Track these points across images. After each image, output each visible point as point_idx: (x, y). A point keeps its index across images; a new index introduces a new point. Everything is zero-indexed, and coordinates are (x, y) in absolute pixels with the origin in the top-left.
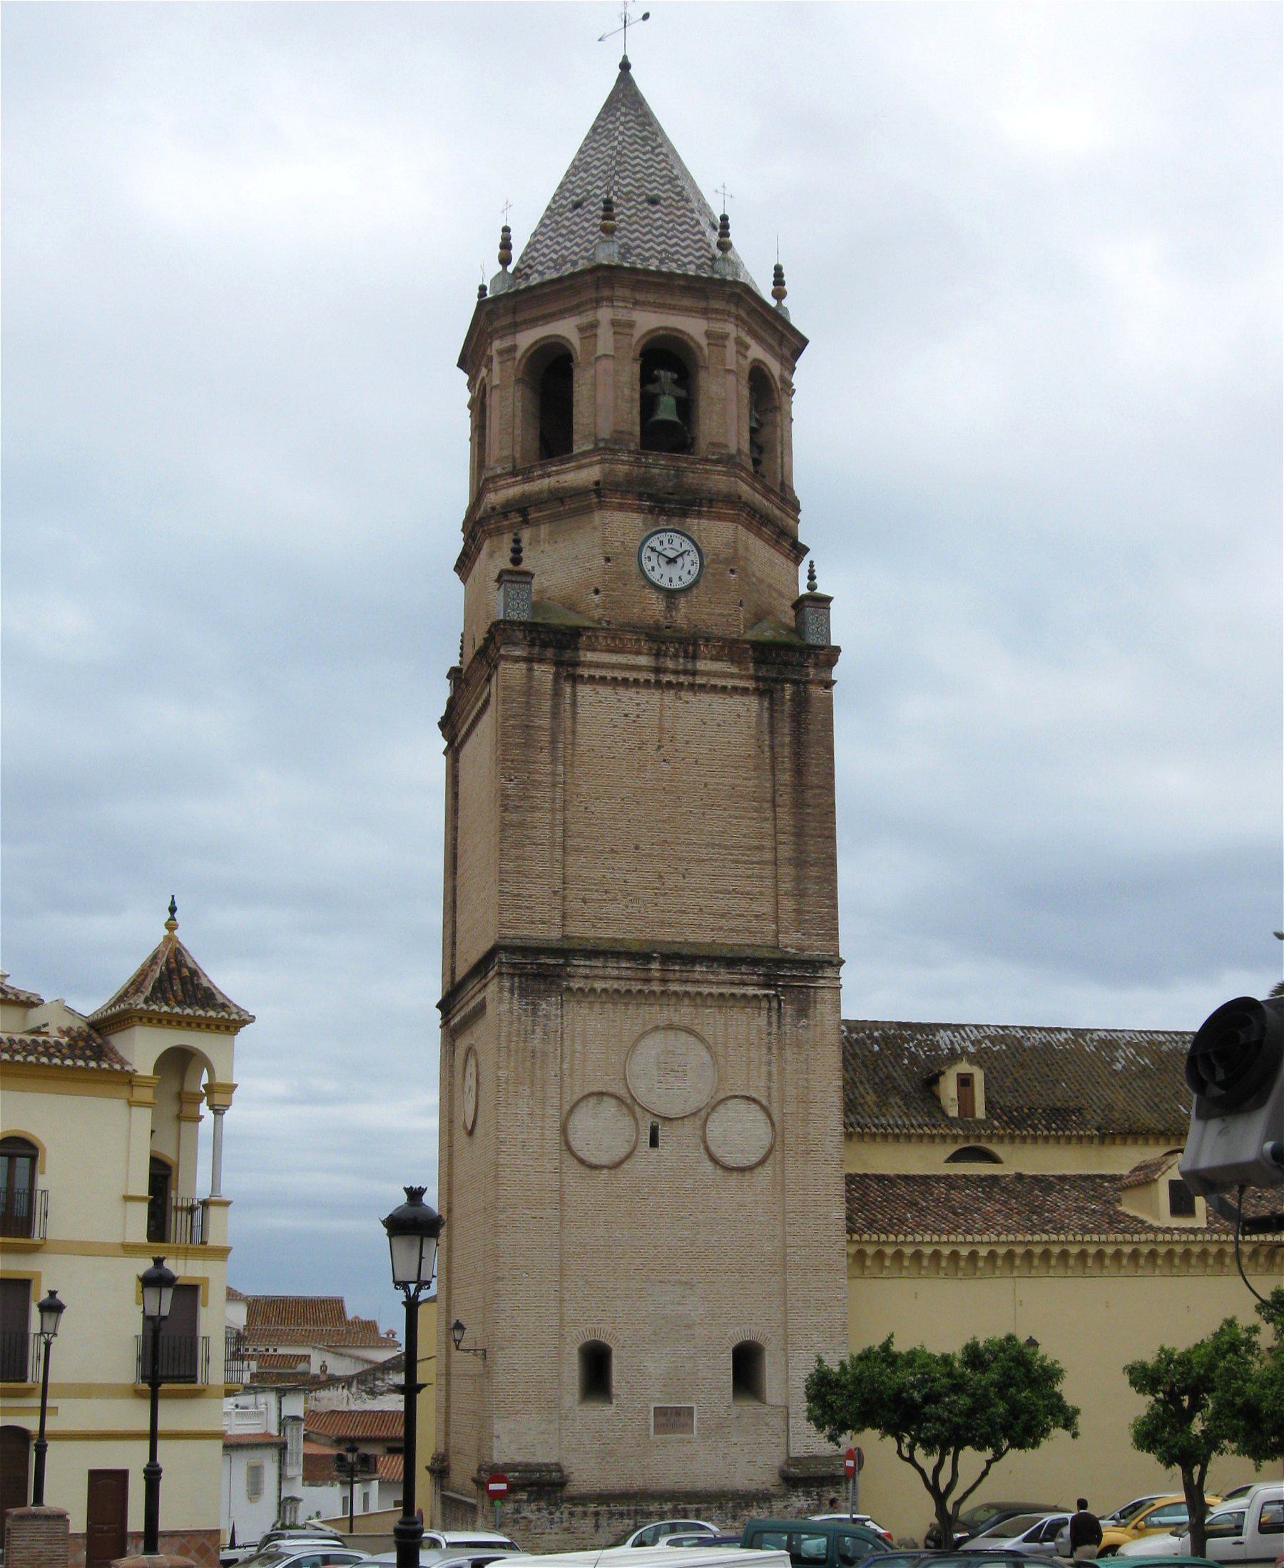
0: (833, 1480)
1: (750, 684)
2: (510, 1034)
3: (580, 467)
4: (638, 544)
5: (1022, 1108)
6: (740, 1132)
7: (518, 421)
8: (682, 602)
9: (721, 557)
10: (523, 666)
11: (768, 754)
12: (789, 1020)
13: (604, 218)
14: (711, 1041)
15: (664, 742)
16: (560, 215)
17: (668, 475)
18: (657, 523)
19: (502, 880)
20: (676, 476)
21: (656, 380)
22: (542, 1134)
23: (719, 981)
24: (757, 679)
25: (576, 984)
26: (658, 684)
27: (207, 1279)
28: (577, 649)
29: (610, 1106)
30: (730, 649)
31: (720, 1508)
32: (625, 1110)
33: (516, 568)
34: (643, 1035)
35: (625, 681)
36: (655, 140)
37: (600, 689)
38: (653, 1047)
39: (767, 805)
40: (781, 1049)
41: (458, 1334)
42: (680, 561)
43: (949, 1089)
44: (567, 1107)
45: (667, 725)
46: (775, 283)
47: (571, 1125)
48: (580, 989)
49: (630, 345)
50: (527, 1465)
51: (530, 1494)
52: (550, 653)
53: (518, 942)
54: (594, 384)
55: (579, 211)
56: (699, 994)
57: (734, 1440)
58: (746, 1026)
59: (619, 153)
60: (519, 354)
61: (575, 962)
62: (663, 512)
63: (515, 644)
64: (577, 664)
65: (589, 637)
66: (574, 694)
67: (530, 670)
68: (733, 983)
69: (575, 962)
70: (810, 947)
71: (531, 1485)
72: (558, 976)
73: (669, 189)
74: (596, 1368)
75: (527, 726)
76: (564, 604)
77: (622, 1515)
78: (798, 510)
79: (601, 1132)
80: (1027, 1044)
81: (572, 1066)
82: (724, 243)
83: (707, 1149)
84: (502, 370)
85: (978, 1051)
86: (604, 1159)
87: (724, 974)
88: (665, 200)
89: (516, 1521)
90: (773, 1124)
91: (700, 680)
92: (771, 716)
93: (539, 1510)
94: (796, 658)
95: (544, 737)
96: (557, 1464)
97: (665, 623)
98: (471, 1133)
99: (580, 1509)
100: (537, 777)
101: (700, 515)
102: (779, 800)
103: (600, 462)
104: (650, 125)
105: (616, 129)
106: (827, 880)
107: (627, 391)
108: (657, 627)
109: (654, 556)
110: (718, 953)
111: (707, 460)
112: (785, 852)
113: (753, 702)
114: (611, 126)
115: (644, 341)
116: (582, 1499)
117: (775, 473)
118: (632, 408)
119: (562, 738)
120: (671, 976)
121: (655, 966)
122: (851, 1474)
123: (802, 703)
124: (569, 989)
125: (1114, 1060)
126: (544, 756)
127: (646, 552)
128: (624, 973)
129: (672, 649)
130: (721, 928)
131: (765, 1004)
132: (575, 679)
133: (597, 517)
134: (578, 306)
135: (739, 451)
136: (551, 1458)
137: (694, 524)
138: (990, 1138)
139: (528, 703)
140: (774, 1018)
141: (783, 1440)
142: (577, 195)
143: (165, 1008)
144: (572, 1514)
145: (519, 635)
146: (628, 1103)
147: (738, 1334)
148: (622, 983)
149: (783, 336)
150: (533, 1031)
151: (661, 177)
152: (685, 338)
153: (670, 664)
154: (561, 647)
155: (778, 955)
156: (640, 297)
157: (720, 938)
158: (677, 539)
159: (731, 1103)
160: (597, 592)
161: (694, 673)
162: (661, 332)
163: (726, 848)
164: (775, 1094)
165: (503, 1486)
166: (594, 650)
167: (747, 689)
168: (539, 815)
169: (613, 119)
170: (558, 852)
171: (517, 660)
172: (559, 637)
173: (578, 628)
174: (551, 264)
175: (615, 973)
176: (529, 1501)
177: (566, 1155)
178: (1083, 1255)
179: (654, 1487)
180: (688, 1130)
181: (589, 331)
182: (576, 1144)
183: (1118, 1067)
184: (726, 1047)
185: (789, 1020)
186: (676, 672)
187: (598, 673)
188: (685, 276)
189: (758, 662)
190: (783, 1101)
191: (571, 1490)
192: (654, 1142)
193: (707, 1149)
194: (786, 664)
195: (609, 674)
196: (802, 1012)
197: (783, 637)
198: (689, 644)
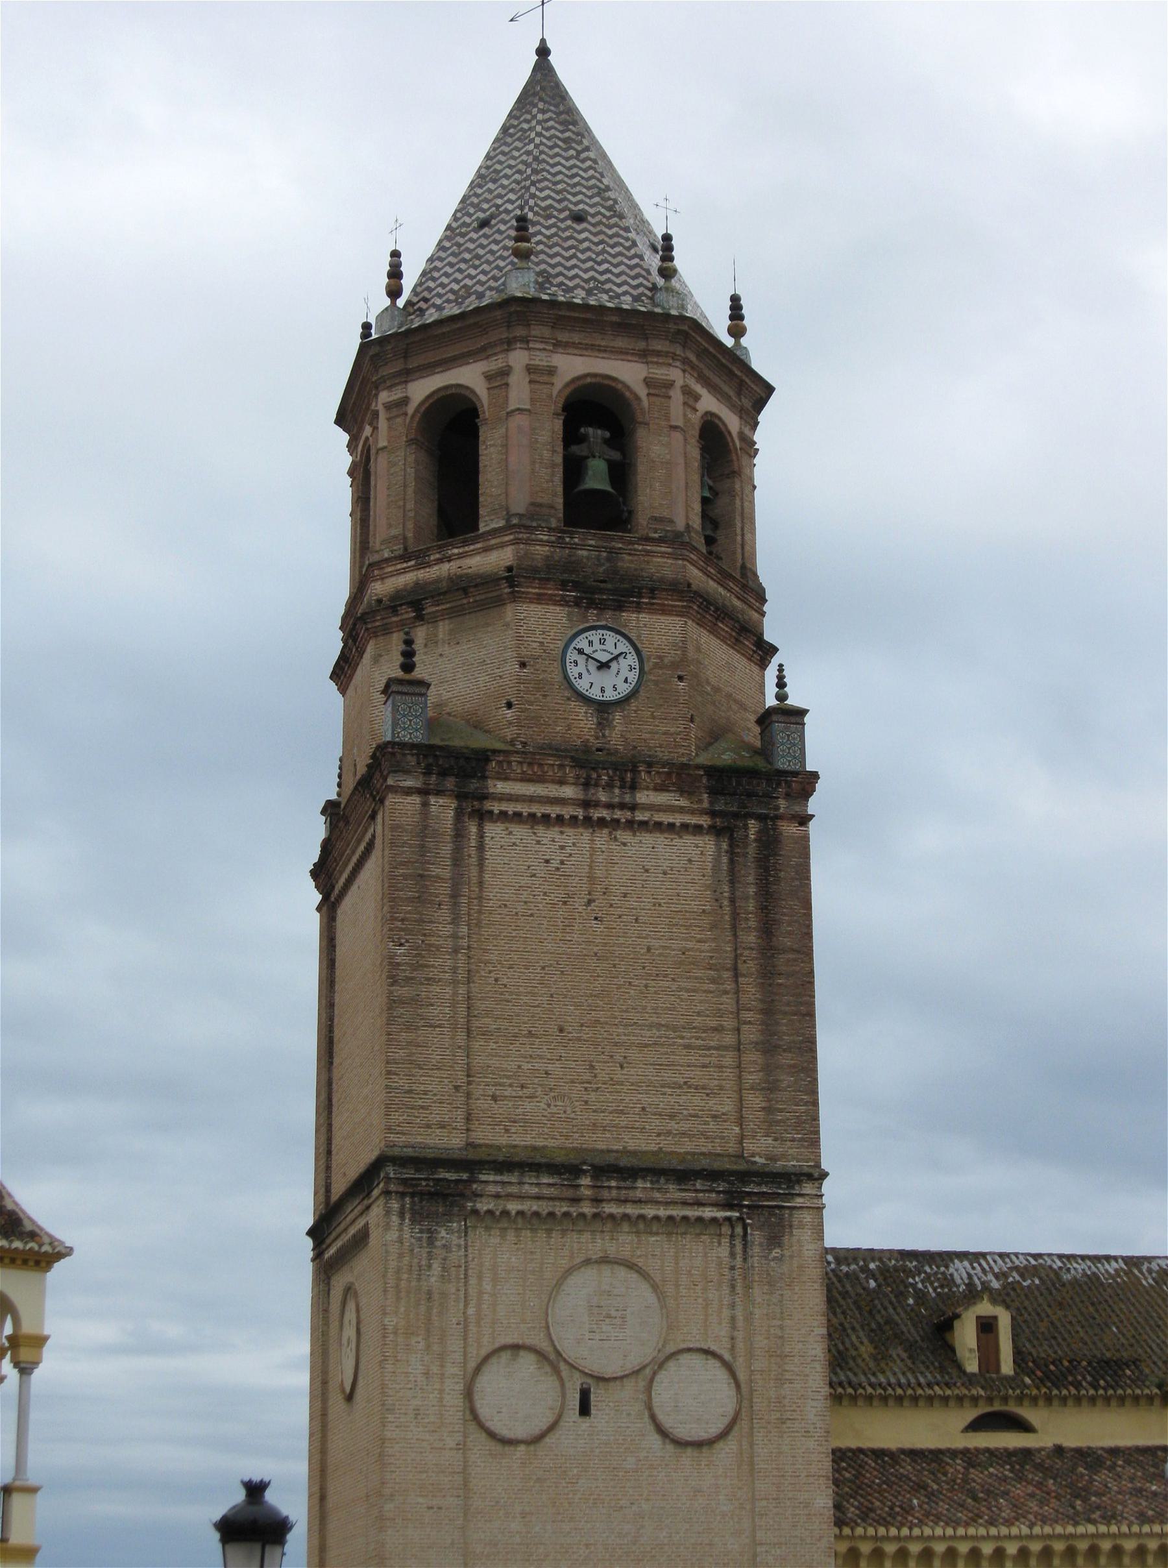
2: (398, 1270)
3: (486, 550)
4: (561, 644)
6: (696, 1396)
7: (410, 491)
9: (666, 661)
10: (417, 799)
14: (658, 1278)
15: (596, 895)
17: (598, 558)
18: (585, 619)
19: (389, 1073)
20: (608, 560)
21: (582, 439)
22: (441, 1399)
23: (666, 1203)
24: (713, 814)
25: (483, 1206)
26: (588, 821)
28: (484, 778)
29: (527, 1362)
30: (679, 776)
32: (548, 1369)
33: (407, 677)
34: (569, 1272)
35: (546, 818)
36: (581, 142)
39: (726, 975)
40: (748, 1287)
42: (614, 665)
43: (966, 1336)
44: (472, 1365)
45: (598, 873)
46: (732, 318)
48: (490, 1212)
52: (450, 783)
53: (409, 1152)
55: (486, 230)
56: (642, 1217)
58: (705, 1256)
59: (536, 159)
60: (411, 409)
61: (483, 1177)
62: (592, 604)
63: (407, 772)
64: (485, 797)
65: (500, 763)
66: (481, 836)
67: (425, 804)
68: (685, 1203)
69: (483, 1177)
70: (784, 1156)
72: (462, 1195)
75: (421, 876)
76: (468, 721)
78: (763, 600)
79: (517, 1396)
83: (653, 1417)
85: (1004, 1287)
86: (520, 1431)
87: (673, 1191)
91: (640, 816)
92: (731, 861)
95: (442, 890)
100: (433, 940)
101: (639, 608)
102: (742, 968)
103: (516, 542)
104: (575, 123)
105: (530, 129)
106: (804, 1070)
109: (581, 660)
110: (665, 1164)
111: (647, 539)
112: (751, 1034)
113: (708, 844)
114: (525, 126)
117: (734, 553)
118: (553, 475)
119: (465, 890)
120: (605, 1194)
121: (585, 1181)
123: (770, 844)
124: (475, 1212)
126: (445, 913)
127: (572, 655)
128: (546, 1191)
129: (605, 776)
130: (669, 1133)
131: (726, 1230)
132: (483, 816)
134: (484, 349)
137: (631, 619)
138: (1020, 1400)
139: (423, 846)
142: (484, 211)
145: (412, 760)
146: (552, 1360)
149: (741, 383)
150: (430, 1266)
152: (619, 386)
153: (603, 797)
154: (464, 775)
155: (742, 1166)
156: (563, 336)
159: (685, 1358)
160: (509, 705)
161: (633, 807)
163: (675, 1029)
164: (740, 1345)
166: (506, 779)
169: (528, 117)
170: (461, 1037)
171: (408, 792)
172: (462, 762)
174: (452, 297)
175: (535, 1190)
177: (472, 1426)
180: (629, 1392)
181: (499, 379)
182: (484, 1412)
184: (677, 1286)
186: (610, 806)
187: (510, 808)
188: (619, 310)
189: (714, 792)
193: (653, 1417)
194: (750, 795)
195: (524, 809)
196: (774, 1240)
197: (746, 760)
198: (627, 770)
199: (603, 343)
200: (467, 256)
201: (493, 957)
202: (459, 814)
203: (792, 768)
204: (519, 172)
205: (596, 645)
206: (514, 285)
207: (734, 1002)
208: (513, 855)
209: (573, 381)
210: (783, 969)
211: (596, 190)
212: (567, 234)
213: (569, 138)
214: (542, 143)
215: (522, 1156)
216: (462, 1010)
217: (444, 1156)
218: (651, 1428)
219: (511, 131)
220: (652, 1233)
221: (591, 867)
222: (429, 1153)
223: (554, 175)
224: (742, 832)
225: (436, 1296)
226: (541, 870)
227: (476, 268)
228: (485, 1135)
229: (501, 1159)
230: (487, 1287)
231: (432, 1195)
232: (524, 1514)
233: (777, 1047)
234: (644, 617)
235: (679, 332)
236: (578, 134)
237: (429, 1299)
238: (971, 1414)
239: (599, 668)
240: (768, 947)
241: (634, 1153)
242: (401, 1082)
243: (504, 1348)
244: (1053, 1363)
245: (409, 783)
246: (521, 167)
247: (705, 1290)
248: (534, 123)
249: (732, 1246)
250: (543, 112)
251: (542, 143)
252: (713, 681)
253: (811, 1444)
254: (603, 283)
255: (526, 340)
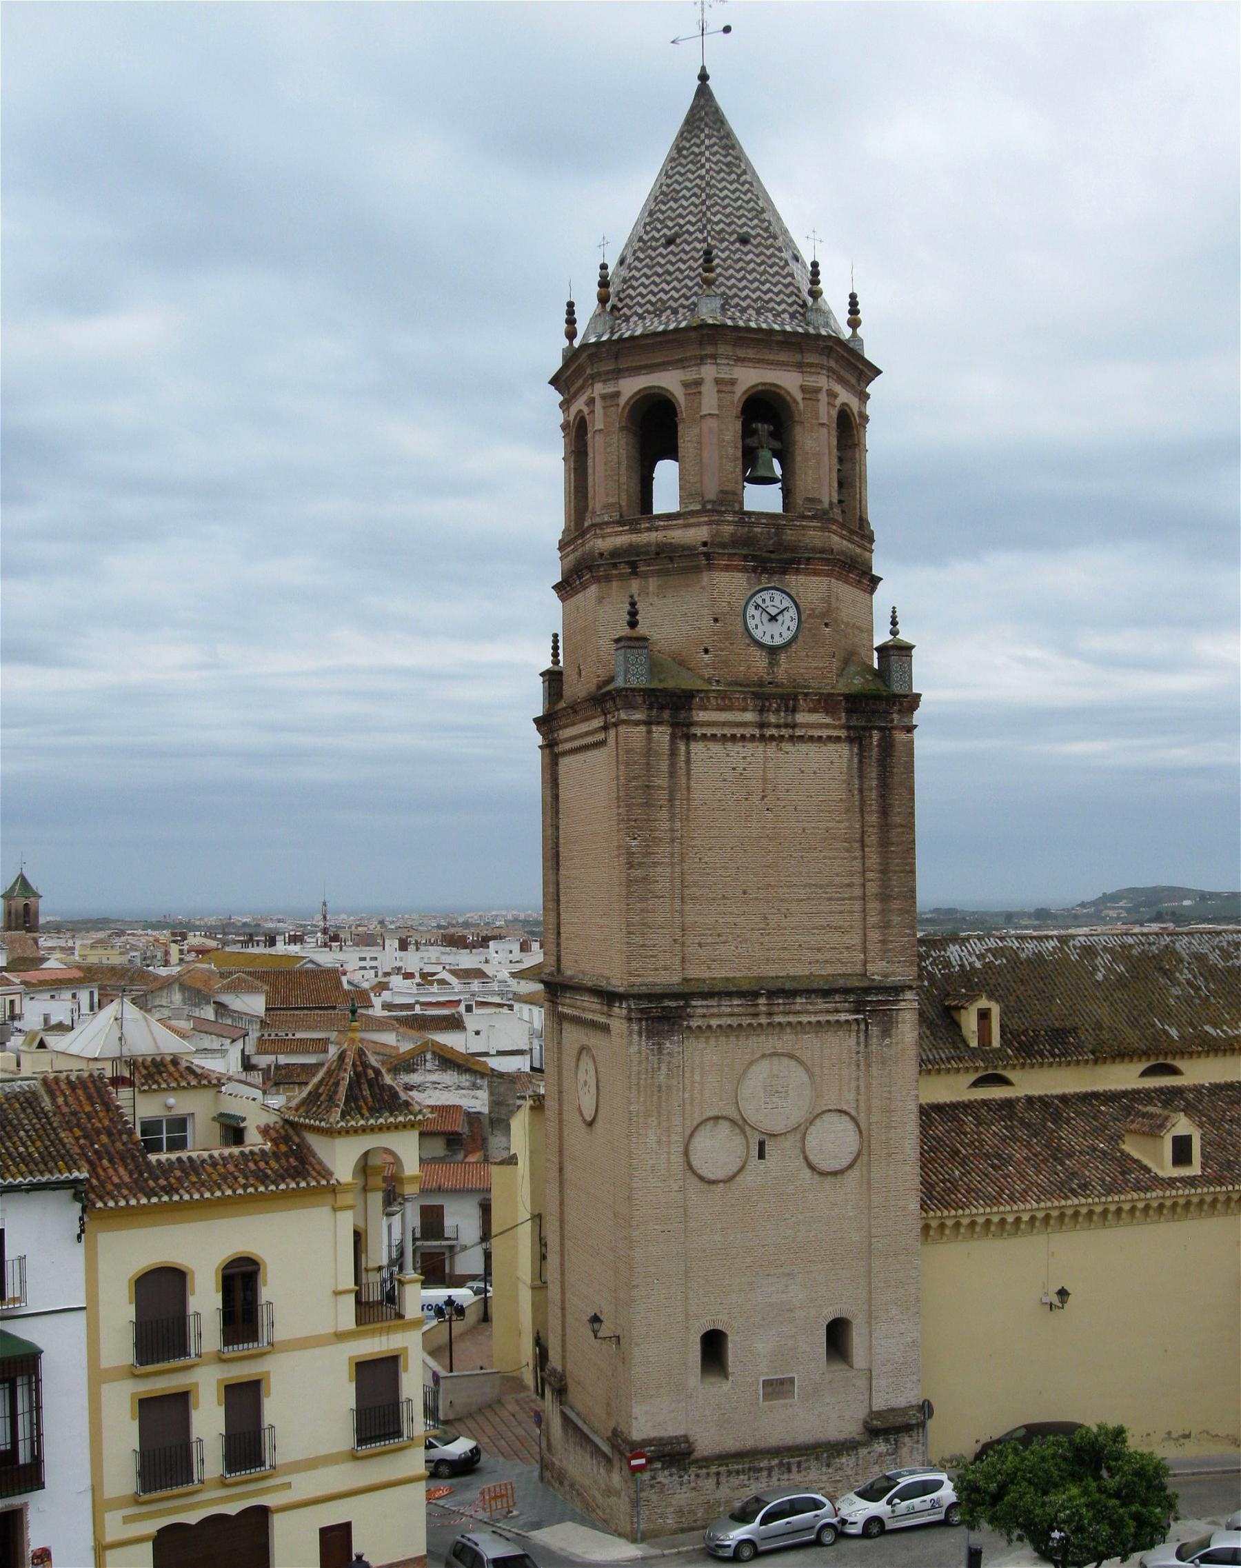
0: (907, 1428)
1: (843, 733)
2: (639, 1073)
3: (686, 526)
4: (743, 603)
5: (1027, 1030)
6: (834, 1141)
7: (623, 470)
8: (783, 657)
9: (817, 612)
10: (643, 728)
11: (857, 797)
12: (875, 1040)
13: (706, 270)
14: (809, 1063)
15: (768, 792)
16: (655, 249)
17: (768, 533)
18: (760, 582)
19: (629, 933)
20: (776, 534)
21: (754, 432)
22: (668, 1159)
23: (814, 1010)
24: (848, 728)
25: (694, 1023)
26: (763, 738)
27: (406, 1348)
28: (691, 709)
29: (724, 1128)
30: (826, 703)
31: (817, 1459)
32: (738, 1131)
33: (633, 633)
34: (751, 1063)
35: (733, 737)
36: (739, 166)
37: (711, 745)
38: (760, 1072)
39: (856, 845)
40: (868, 1065)
41: (596, 1326)
42: (780, 618)
43: (969, 1022)
44: (688, 1132)
45: (769, 776)
46: (851, 312)
47: (692, 1147)
48: (699, 1027)
49: (732, 403)
50: (661, 1439)
51: (663, 1463)
52: (666, 715)
53: (644, 990)
54: (700, 443)
55: (672, 247)
56: (800, 1023)
57: (827, 1400)
58: (841, 1045)
59: (708, 184)
60: (623, 400)
61: (694, 1003)
62: (765, 570)
63: (635, 708)
64: (692, 724)
65: (701, 699)
66: (688, 752)
67: (649, 732)
68: (828, 1012)
69: (694, 1003)
70: (893, 974)
71: (664, 1456)
72: (680, 1017)
73: (760, 233)
74: (713, 1347)
75: (648, 786)
76: (674, 659)
77: (738, 1472)
78: (872, 540)
79: (717, 1151)
80: (1023, 956)
81: (691, 1096)
82: (815, 292)
83: (806, 1158)
84: (605, 415)
85: (984, 966)
86: (720, 1174)
87: (821, 1004)
88: (755, 237)
89: (652, 1486)
90: (860, 1132)
91: (799, 732)
92: (860, 762)
93: (671, 1475)
94: (883, 706)
95: (663, 795)
96: (686, 1437)
97: (768, 678)
98: (590, 1124)
99: (704, 1471)
100: (657, 834)
101: (798, 572)
102: (867, 841)
103: (709, 523)
104: (733, 147)
105: (702, 154)
106: (907, 912)
107: (731, 451)
108: (761, 684)
109: (757, 613)
110: (815, 986)
111: (804, 517)
112: (873, 888)
113: (844, 749)
114: (696, 150)
115: (745, 398)
116: (706, 1461)
117: (855, 508)
118: (735, 467)
119: (678, 796)
120: (775, 1009)
121: (762, 1001)
122: (922, 1425)
123: (887, 747)
124: (689, 1027)
125: (1095, 969)
126: (664, 814)
127: (751, 610)
128: (736, 1010)
129: (774, 703)
130: (817, 961)
131: (854, 1027)
132: (689, 738)
133: (705, 577)
134: (681, 360)
135: (831, 503)
136: (680, 1432)
137: (796, 582)
138: (1005, 1067)
139: (648, 764)
140: (862, 1039)
141: (867, 1397)
142: (670, 229)
143: (362, 1122)
144: (697, 1476)
145: (639, 700)
146: (740, 1124)
147: (830, 1313)
148: (734, 1018)
149: (861, 372)
150: (659, 1068)
151: (749, 211)
152: (782, 392)
153: (773, 719)
154: (676, 709)
155: (865, 984)
156: (742, 353)
157: (817, 970)
158: (778, 596)
159: (826, 1117)
160: (706, 651)
161: (794, 726)
162: (760, 388)
163: (821, 887)
164: (862, 1104)
165: (643, 1461)
166: (706, 709)
167: (839, 737)
168: (659, 869)
169: (698, 141)
170: (678, 902)
171: (637, 723)
172: (675, 699)
173: (691, 691)
174: (651, 309)
175: (729, 1010)
176: (663, 1469)
177: (689, 1174)
178: (1105, 1212)
179: (762, 1445)
180: (790, 1143)
181: (694, 387)
182: (696, 1163)
183: (1099, 977)
184: (822, 1067)
185: (875, 1040)
186: (778, 726)
187: (709, 731)
188: (784, 332)
189: (849, 712)
190: (869, 1110)
191: (697, 1455)
192: (761, 1156)
193: (806, 1158)
194: (873, 712)
195: (718, 732)
196: (886, 1033)
197: (874, 686)
198: (789, 700)
199: (771, 357)
200: (660, 271)
201: (697, 842)
202: (673, 737)
203: (902, 692)
204: (695, 195)
205: (768, 602)
206: (704, 310)
207: (860, 865)
208: (715, 767)
209: (749, 389)
210: (894, 840)
211: (754, 213)
212: (737, 256)
213: (730, 162)
214: (711, 168)
215: (720, 987)
216: (678, 883)
217: (668, 991)
218: (804, 1165)
219: (685, 152)
220: (806, 1033)
221: (764, 771)
222: (658, 990)
223: (723, 199)
224: (868, 740)
225: (664, 1088)
226: (729, 775)
227: (668, 283)
228: (695, 972)
229: (706, 990)
230: (697, 1078)
231: (660, 1019)
232: (723, 1229)
233: (890, 896)
234: (802, 578)
235: (827, 347)
236: (737, 158)
237: (659, 1091)
238: (973, 1077)
239: (770, 620)
240: (885, 827)
241: (794, 978)
242: (638, 939)
243: (709, 1119)
244: (1023, 1033)
245: (638, 716)
246: (696, 190)
247: (840, 1069)
248: (703, 148)
249: (858, 1037)
250: (709, 137)
251: (711, 168)
252: (845, 620)
253: (908, 1168)
254: (767, 302)
255: (714, 357)
